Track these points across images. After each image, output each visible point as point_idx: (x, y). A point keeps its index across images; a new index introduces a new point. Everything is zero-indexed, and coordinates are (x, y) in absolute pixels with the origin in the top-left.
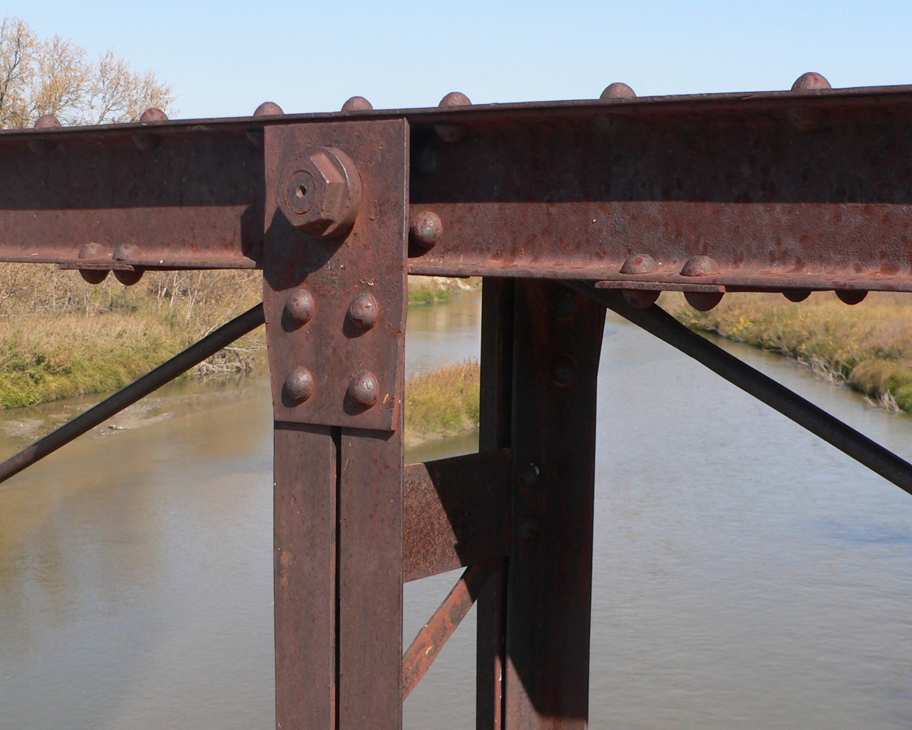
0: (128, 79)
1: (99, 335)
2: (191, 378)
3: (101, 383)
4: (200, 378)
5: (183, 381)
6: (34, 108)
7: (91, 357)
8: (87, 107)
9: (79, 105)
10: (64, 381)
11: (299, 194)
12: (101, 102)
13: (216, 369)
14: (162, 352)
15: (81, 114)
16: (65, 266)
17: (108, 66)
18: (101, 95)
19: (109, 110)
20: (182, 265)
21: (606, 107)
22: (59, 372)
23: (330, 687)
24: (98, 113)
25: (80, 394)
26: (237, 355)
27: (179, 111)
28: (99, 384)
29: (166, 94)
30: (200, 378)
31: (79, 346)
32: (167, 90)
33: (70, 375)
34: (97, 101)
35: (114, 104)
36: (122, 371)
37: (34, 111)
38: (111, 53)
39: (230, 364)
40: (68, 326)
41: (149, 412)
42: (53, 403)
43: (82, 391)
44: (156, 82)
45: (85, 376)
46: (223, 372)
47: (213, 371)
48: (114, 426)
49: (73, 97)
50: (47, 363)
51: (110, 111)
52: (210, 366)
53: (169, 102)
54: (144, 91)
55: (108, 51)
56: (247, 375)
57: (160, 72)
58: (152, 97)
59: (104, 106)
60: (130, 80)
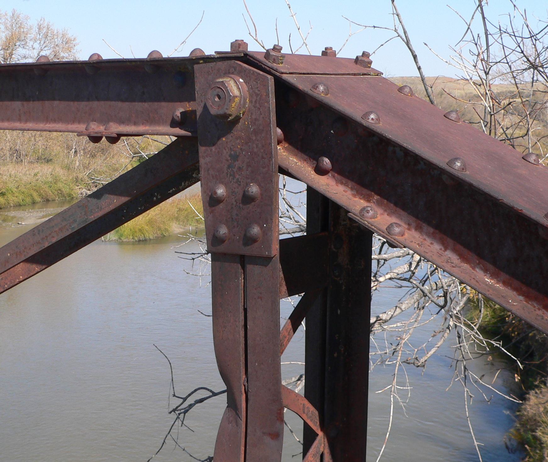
0: (54, 33)
1: (25, 174)
2: (76, 198)
3: (23, 200)
5: (71, 199)
9: (27, 48)
11: (217, 99)
12: (38, 46)
14: (59, 184)
15: (28, 52)
16: (80, 134)
17: (42, 26)
18: (38, 42)
20: (136, 133)
21: (50, 64)
23: (424, 360)
25: (11, 207)
28: (22, 201)
29: (73, 41)
31: (12, 180)
33: (5, 196)
34: (36, 45)
35: (45, 47)
36: (35, 195)
38: (44, 18)
40: (8, 170)
43: (12, 205)
44: (68, 34)
45: (14, 197)
48: (20, 223)
49: (23, 43)
53: (76, 45)
54: (62, 40)
55: (42, 17)
57: (71, 28)
59: (40, 48)
60: (55, 33)
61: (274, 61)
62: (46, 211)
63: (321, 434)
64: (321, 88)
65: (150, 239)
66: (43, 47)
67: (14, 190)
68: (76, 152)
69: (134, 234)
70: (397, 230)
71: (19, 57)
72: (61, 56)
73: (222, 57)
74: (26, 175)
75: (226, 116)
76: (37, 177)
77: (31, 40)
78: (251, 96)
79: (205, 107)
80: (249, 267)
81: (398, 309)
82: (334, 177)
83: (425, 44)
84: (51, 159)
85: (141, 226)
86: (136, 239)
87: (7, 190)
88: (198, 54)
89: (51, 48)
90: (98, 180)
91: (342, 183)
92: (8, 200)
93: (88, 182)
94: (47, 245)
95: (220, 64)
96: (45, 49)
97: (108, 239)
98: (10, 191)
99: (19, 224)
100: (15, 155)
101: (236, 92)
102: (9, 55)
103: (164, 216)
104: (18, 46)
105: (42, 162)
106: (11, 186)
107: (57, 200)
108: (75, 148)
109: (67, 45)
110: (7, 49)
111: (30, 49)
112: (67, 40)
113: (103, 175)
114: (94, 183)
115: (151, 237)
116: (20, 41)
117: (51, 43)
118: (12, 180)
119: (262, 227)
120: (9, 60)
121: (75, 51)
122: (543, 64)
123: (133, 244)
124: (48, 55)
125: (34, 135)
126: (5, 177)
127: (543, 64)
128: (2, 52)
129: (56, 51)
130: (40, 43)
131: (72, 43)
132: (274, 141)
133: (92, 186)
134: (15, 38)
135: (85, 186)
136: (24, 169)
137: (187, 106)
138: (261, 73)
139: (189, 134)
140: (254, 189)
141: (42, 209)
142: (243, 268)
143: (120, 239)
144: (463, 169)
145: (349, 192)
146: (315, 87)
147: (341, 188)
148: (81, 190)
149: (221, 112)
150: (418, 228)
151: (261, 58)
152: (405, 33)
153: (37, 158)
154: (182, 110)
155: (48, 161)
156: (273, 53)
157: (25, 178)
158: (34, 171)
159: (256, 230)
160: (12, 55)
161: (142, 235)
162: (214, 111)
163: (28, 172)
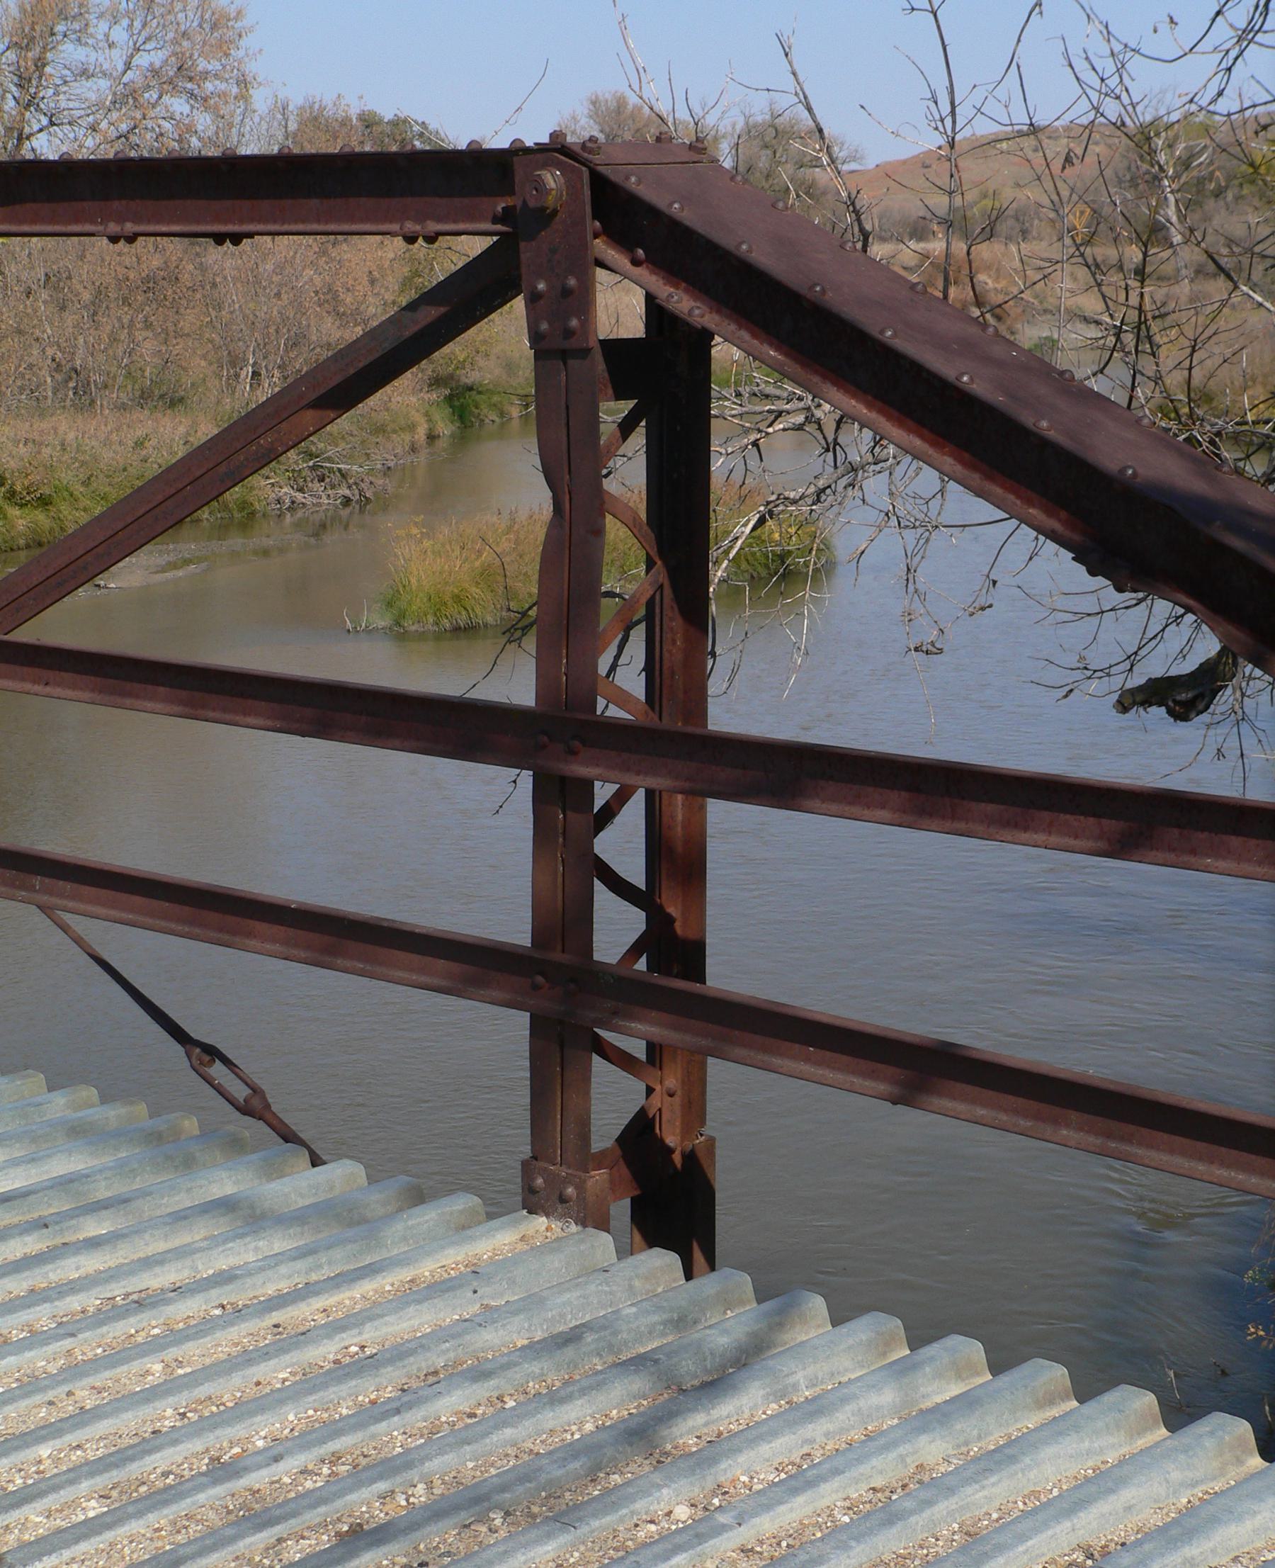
1: (107, 443)
2: (264, 515)
4: (279, 516)
6: (8, 48)
7: (89, 479)
8: (103, 44)
9: (90, 41)
10: (40, 516)
11: (534, 192)
13: (309, 501)
15: (93, 56)
18: (125, 22)
19: (139, 50)
22: (29, 501)
24: (121, 56)
26: (343, 476)
27: (261, 50)
29: (236, 19)
30: (279, 516)
31: (69, 461)
32: (239, 13)
33: (50, 507)
34: (119, 34)
35: (148, 39)
37: (9, 52)
39: (333, 491)
40: (55, 429)
41: (169, 563)
42: (21, 552)
46: (319, 504)
47: (303, 504)
49: (76, 26)
50: (8, 487)
51: (141, 53)
52: (299, 496)
56: (362, 511)
58: (214, 27)
59: (131, 43)
61: (590, 153)
62: (175, 550)
63: (659, 563)
64: (633, 179)
65: (486, 625)
66: (141, 41)
67: (78, 489)
68: (256, 374)
69: (439, 610)
70: (697, 312)
71: (66, 72)
72: (200, 68)
73: (541, 149)
74: (111, 445)
75: (544, 209)
76: (144, 452)
77: (101, 16)
78: (567, 188)
79: (525, 202)
80: (571, 362)
81: (812, 486)
82: (647, 267)
83: (862, 107)
84: (183, 398)
85: (457, 587)
86: (446, 624)
87: (57, 490)
88: (518, 145)
89: (165, 42)
90: (329, 460)
91: (655, 274)
92: (59, 518)
93: (298, 465)
94: (352, 371)
95: (539, 156)
96: (148, 47)
97: (363, 625)
98: (65, 493)
99: (98, 586)
100: (72, 384)
101: (553, 185)
102: (36, 66)
103: (527, 559)
104: (60, 38)
105: (155, 407)
106: (69, 477)
107: (207, 519)
108: (255, 364)
109: (215, 34)
110: (27, 45)
111: (101, 45)
112: (216, 16)
113: (343, 445)
114: (313, 468)
115: (489, 619)
116: (66, 19)
117: (164, 26)
118: (69, 461)
119: (579, 319)
120: (34, 82)
121: (241, 53)
122: (1138, 124)
123: (439, 636)
124: (157, 64)
125: (126, 321)
126: (46, 451)
127: (1138, 124)
128: (11, 56)
129: (183, 54)
130: (131, 26)
131: (233, 27)
132: (589, 236)
133: (309, 479)
134: (52, 10)
135: (289, 479)
136: (103, 427)
137: (510, 201)
138: (577, 165)
139: (511, 230)
140: (572, 282)
141: (165, 547)
142: (565, 364)
143: (398, 624)
144: (750, 251)
145: (661, 282)
146: (627, 178)
147: (654, 278)
148: (277, 489)
149: (539, 205)
150: (718, 312)
151: (578, 149)
152: (805, 97)
153: (138, 394)
154: (504, 205)
155: (175, 402)
156: (589, 145)
157: (107, 455)
158: (132, 431)
159: (574, 323)
160: (44, 65)
161: (464, 613)
162: (532, 204)
163: (114, 437)
